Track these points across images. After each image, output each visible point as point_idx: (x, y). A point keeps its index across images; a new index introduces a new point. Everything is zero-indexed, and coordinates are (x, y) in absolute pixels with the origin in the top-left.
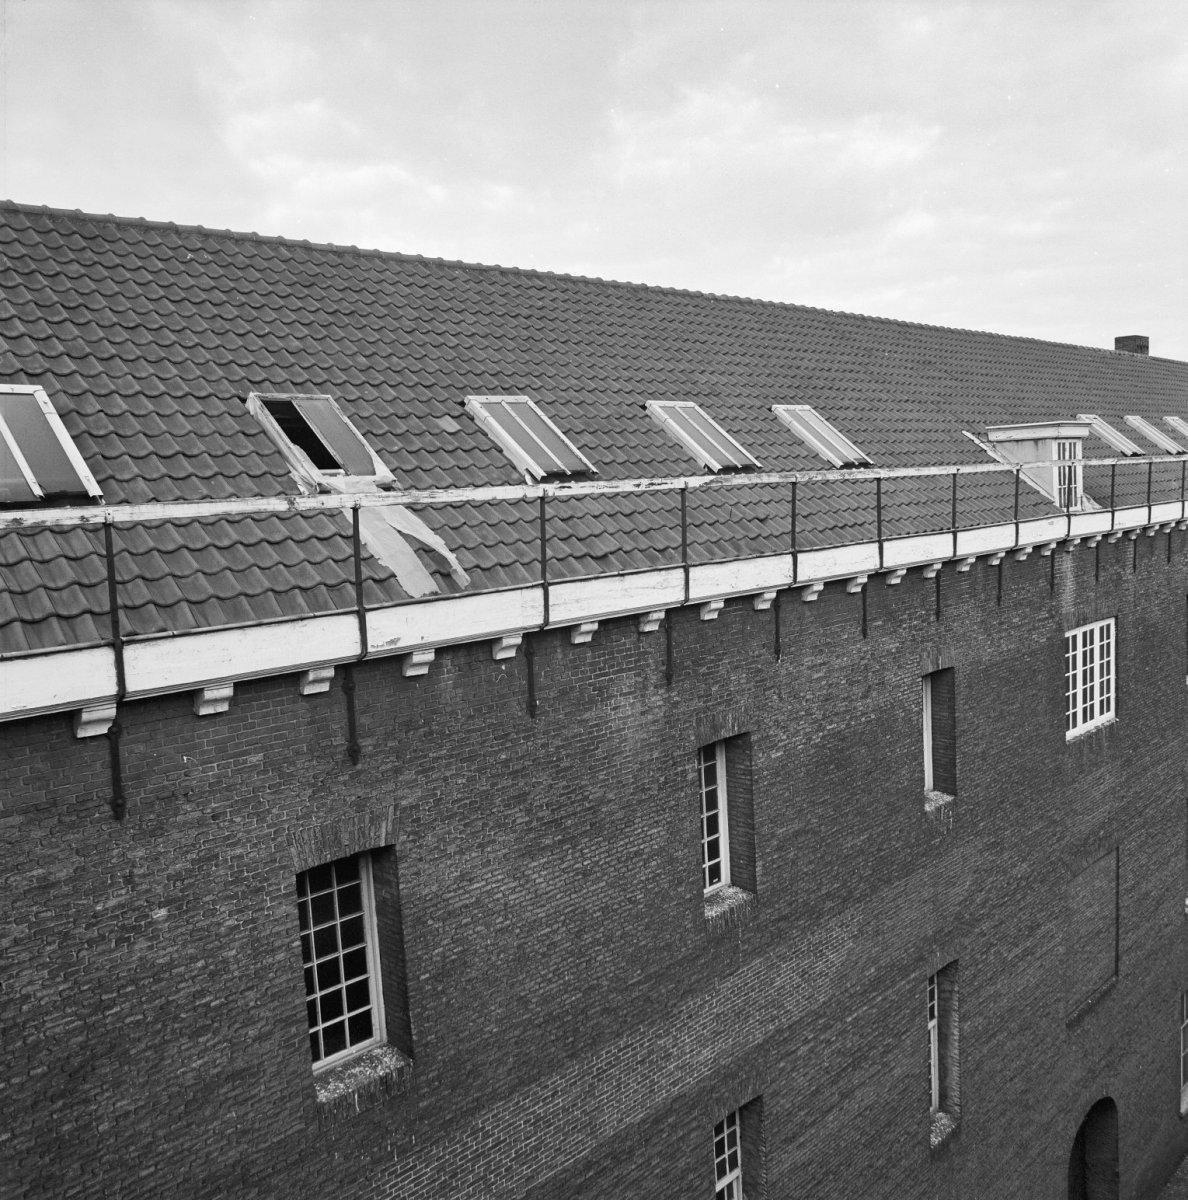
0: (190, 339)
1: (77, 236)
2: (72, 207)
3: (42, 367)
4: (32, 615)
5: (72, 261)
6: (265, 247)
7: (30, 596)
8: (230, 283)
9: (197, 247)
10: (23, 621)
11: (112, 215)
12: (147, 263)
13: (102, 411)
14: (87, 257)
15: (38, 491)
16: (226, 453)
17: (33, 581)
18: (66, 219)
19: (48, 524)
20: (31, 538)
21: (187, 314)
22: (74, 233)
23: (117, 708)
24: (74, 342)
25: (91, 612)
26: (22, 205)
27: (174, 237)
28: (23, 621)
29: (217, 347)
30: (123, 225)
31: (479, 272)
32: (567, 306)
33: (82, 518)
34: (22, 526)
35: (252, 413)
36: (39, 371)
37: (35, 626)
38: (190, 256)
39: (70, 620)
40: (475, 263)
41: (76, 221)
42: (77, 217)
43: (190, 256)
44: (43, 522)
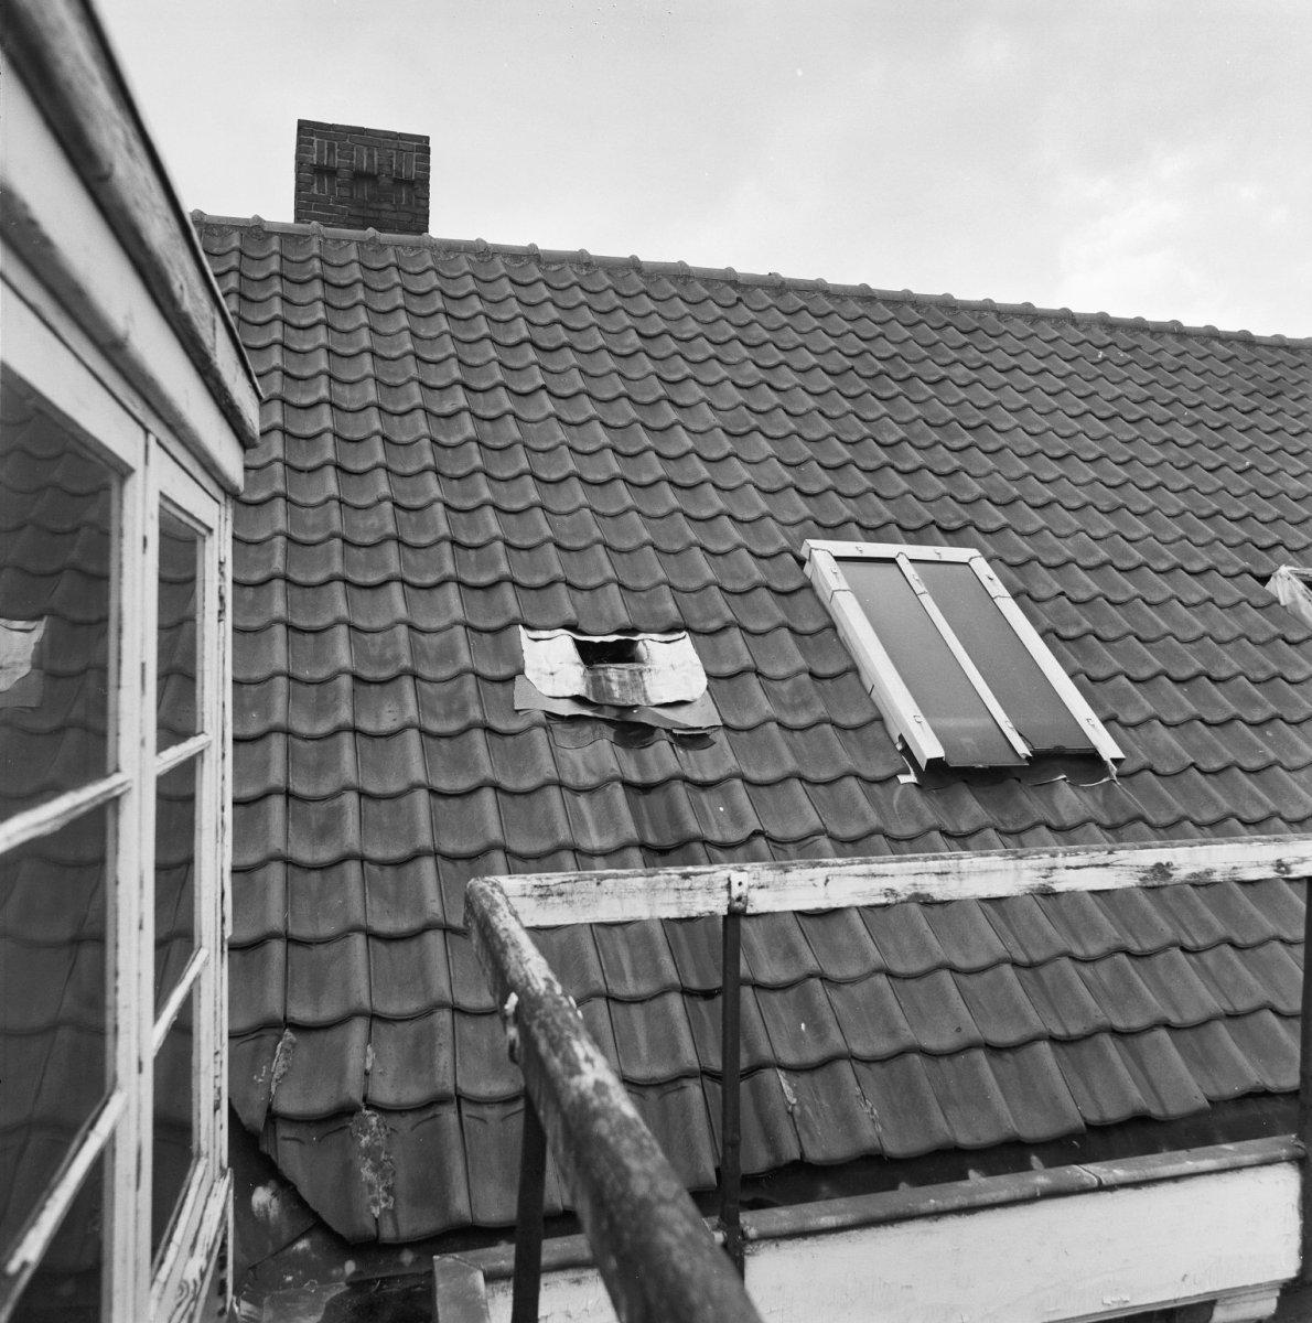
0: (892, 431)
1: (952, 328)
2: (673, 259)
3: (959, 517)
4: (1063, 1025)
5: (955, 362)
6: (1020, 321)
7: (1045, 972)
8: (891, 346)
9: (1055, 336)
10: (1053, 1039)
11: (909, 292)
12: (484, 289)
13: (1063, 594)
14: (971, 356)
15: (1022, 749)
16: (1273, 677)
17: (1048, 940)
18: (933, 308)
19: (1217, 877)
20: (1014, 837)
21: (853, 392)
22: (948, 325)
23: (1280, 1300)
24: (988, 479)
25: (1168, 1026)
26: (879, 291)
27: (533, 267)
28: (1053, 1039)
29: (1188, 488)
30: (1004, 314)
31: (732, 288)
32: (1277, 373)
33: (1279, 864)
34: (1171, 881)
35: (1283, 603)
36: (956, 524)
37: (1070, 1049)
38: (1101, 354)
39: (1129, 1040)
40: (1237, 330)
41: (946, 310)
42: (947, 305)
43: (1101, 354)
44: (1209, 872)
